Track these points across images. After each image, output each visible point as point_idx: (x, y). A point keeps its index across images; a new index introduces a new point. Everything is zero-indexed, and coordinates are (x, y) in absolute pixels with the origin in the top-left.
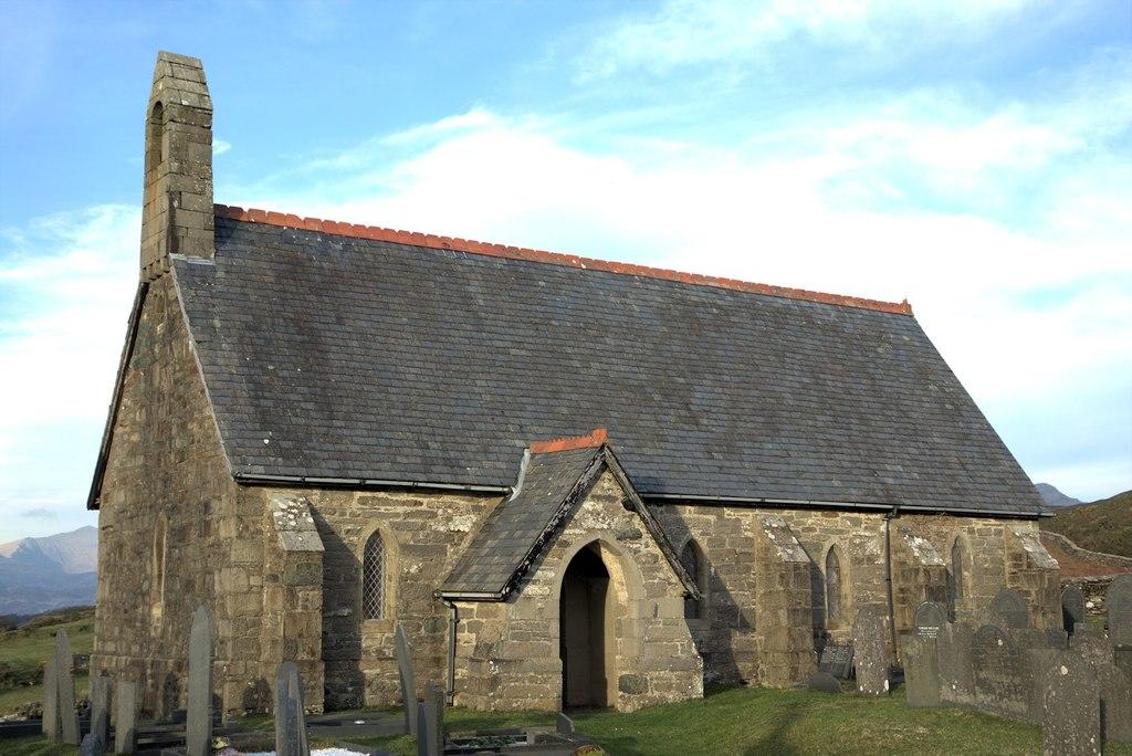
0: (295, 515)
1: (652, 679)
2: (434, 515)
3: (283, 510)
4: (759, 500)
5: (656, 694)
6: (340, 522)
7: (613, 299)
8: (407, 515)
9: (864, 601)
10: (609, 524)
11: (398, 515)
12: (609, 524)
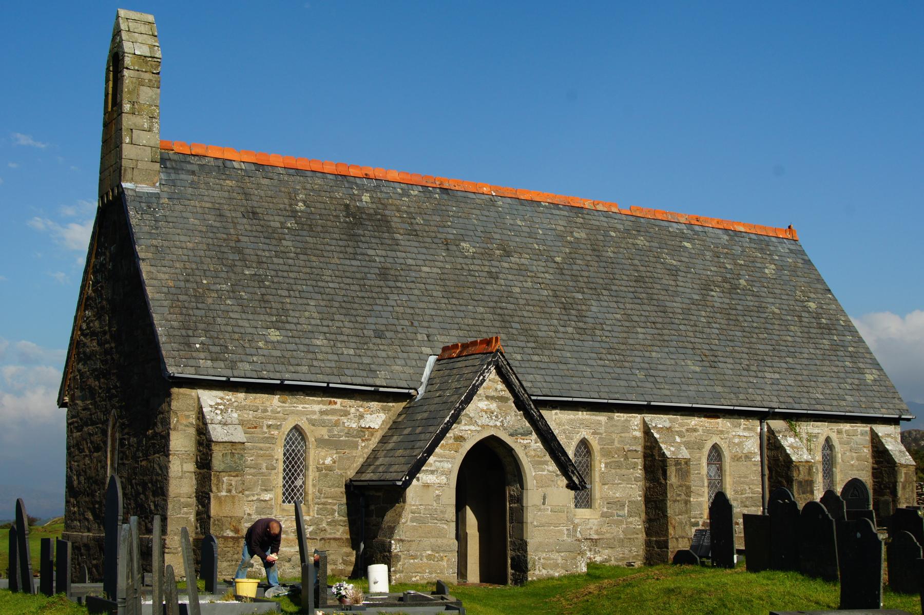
0: (221, 410)
1: (539, 559)
2: (346, 413)
3: (211, 406)
4: (646, 403)
5: (544, 572)
6: (263, 418)
7: (519, 223)
8: (322, 413)
9: (742, 494)
10: (502, 422)
11: (314, 413)
12: (502, 422)
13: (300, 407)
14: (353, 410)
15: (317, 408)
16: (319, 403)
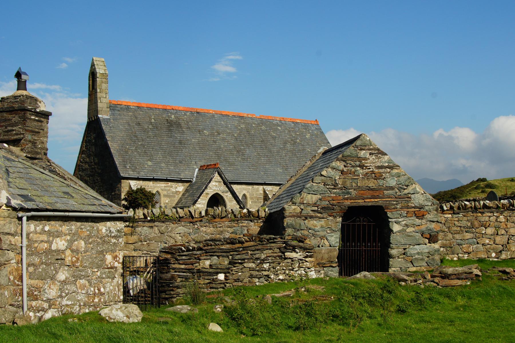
8: (165, 187)
11: (162, 187)
13: (158, 185)
14: (174, 186)
15: (163, 185)
16: (164, 184)
